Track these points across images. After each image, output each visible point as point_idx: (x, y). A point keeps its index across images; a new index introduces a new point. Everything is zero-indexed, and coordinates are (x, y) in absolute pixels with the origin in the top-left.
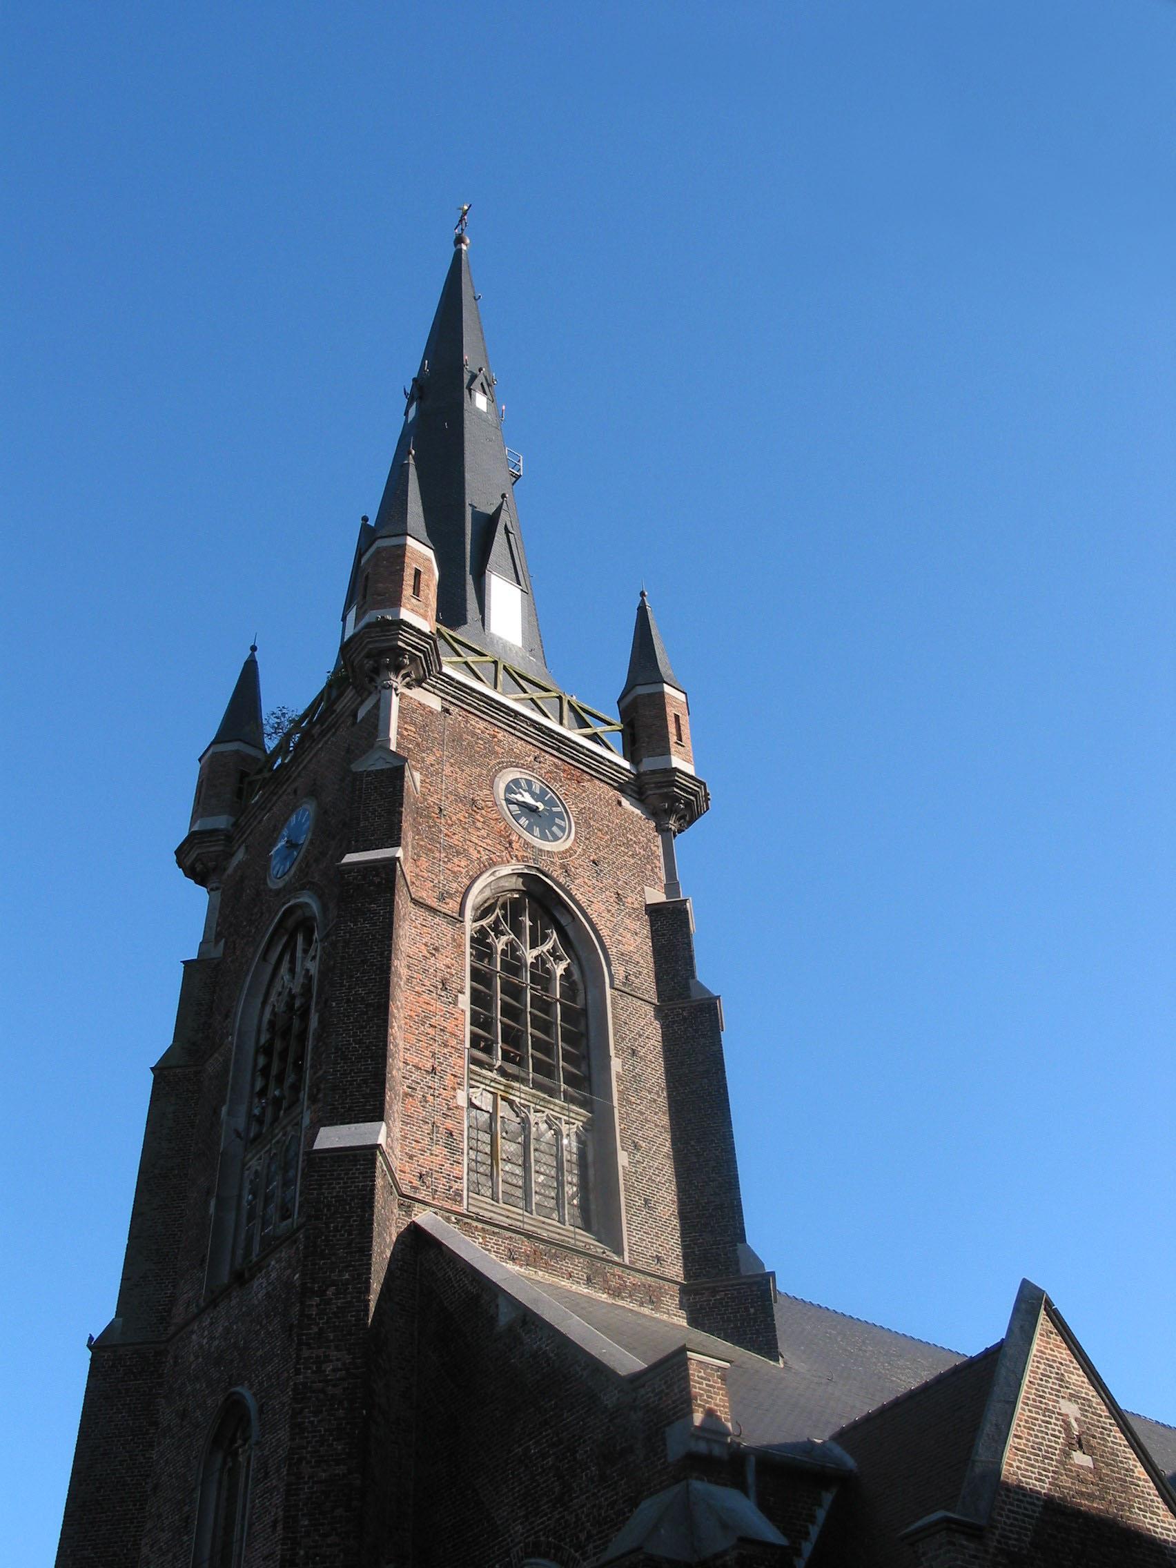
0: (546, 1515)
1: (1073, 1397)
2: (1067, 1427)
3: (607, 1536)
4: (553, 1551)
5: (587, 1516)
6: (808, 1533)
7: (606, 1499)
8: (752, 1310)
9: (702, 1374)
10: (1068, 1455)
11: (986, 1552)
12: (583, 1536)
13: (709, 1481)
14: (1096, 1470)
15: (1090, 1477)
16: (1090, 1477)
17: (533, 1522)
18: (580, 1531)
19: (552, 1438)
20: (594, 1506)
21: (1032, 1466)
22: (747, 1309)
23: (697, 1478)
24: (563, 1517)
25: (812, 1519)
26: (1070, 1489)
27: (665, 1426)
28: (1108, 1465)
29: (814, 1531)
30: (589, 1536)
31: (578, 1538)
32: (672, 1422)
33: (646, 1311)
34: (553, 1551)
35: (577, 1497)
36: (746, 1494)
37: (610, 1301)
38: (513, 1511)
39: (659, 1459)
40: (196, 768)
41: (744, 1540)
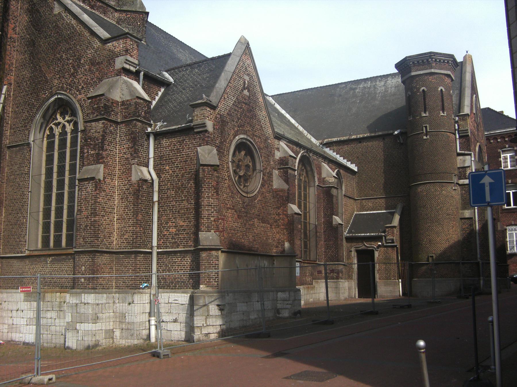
0: (67, 78)
1: (248, 75)
2: (244, 83)
3: (89, 88)
4: (68, 90)
5: (83, 81)
6: (155, 99)
7: (90, 77)
8: (139, 23)
9: (131, 43)
10: (243, 91)
11: (215, 114)
12: (80, 87)
13: (128, 78)
14: (249, 97)
15: (247, 98)
16: (247, 98)
17: (62, 80)
18: (79, 86)
19: (72, 54)
20: (85, 78)
21: (233, 92)
22: (137, 23)
23: (124, 76)
24: (73, 80)
25: (157, 94)
26: (241, 100)
27: (115, 57)
28: (252, 96)
29: (157, 98)
30: (83, 88)
31: (78, 87)
32: (119, 56)
33: (102, 16)
34: (68, 90)
35: (79, 75)
36: (139, 84)
37: (90, 10)
38: (54, 75)
39: (112, 68)
40: (498, 110)
41: (138, 98)
